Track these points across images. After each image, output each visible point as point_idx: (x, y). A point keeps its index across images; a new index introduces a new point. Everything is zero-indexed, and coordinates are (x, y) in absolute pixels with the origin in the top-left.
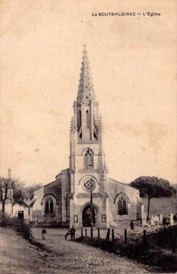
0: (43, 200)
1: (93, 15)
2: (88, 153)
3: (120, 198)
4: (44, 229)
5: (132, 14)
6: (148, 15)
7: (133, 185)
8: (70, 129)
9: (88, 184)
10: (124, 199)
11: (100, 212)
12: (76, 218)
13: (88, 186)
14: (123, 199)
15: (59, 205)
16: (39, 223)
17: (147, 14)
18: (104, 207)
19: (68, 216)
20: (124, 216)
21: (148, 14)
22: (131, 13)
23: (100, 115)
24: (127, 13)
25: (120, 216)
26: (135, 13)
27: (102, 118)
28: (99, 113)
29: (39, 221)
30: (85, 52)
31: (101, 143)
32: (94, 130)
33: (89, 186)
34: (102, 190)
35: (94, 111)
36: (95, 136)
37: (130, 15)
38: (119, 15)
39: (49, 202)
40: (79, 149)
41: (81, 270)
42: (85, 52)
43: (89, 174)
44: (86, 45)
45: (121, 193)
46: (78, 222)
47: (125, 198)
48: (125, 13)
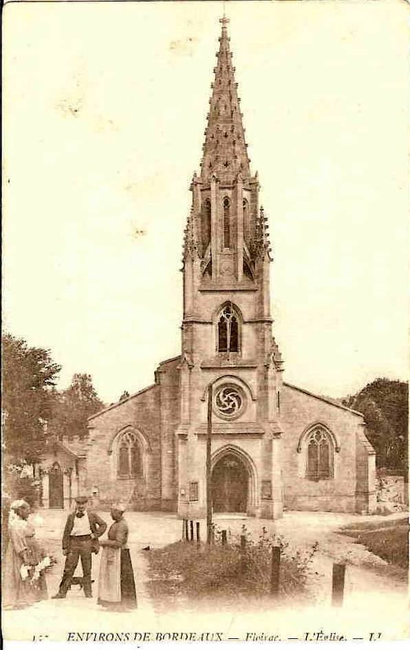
0: (115, 443)
4: (165, 418)
7: (354, 403)
8: (101, 401)
9: (226, 403)
11: (258, 474)
13: (231, 403)
15: (153, 454)
16: (102, 502)
18: (268, 463)
19: (174, 484)
20: (322, 482)
25: (312, 483)
29: (103, 497)
30: (223, 39)
31: (121, 603)
32: (245, 253)
33: (232, 401)
35: (244, 203)
36: (247, 270)
39: (130, 446)
40: (209, 305)
42: (223, 39)
44: (227, 17)
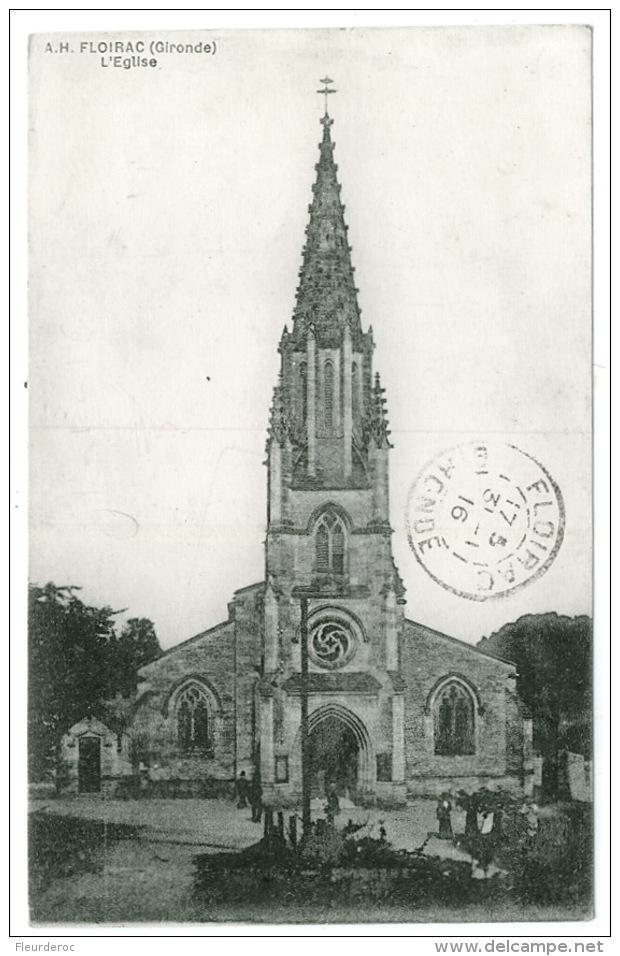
1: (82, 44)
2: (330, 524)
3: (444, 694)
5: (134, 48)
6: (115, 66)
10: (459, 696)
11: (376, 745)
12: (281, 764)
14: (456, 695)
17: (113, 61)
21: (116, 62)
22: (130, 44)
23: (378, 382)
24: (117, 43)
26: (142, 44)
27: (383, 390)
28: (374, 374)
34: (379, 663)
37: (128, 50)
38: (92, 52)
41: (486, 782)
43: (332, 602)
45: (451, 674)
46: (291, 782)
47: (462, 693)
48: (111, 45)
